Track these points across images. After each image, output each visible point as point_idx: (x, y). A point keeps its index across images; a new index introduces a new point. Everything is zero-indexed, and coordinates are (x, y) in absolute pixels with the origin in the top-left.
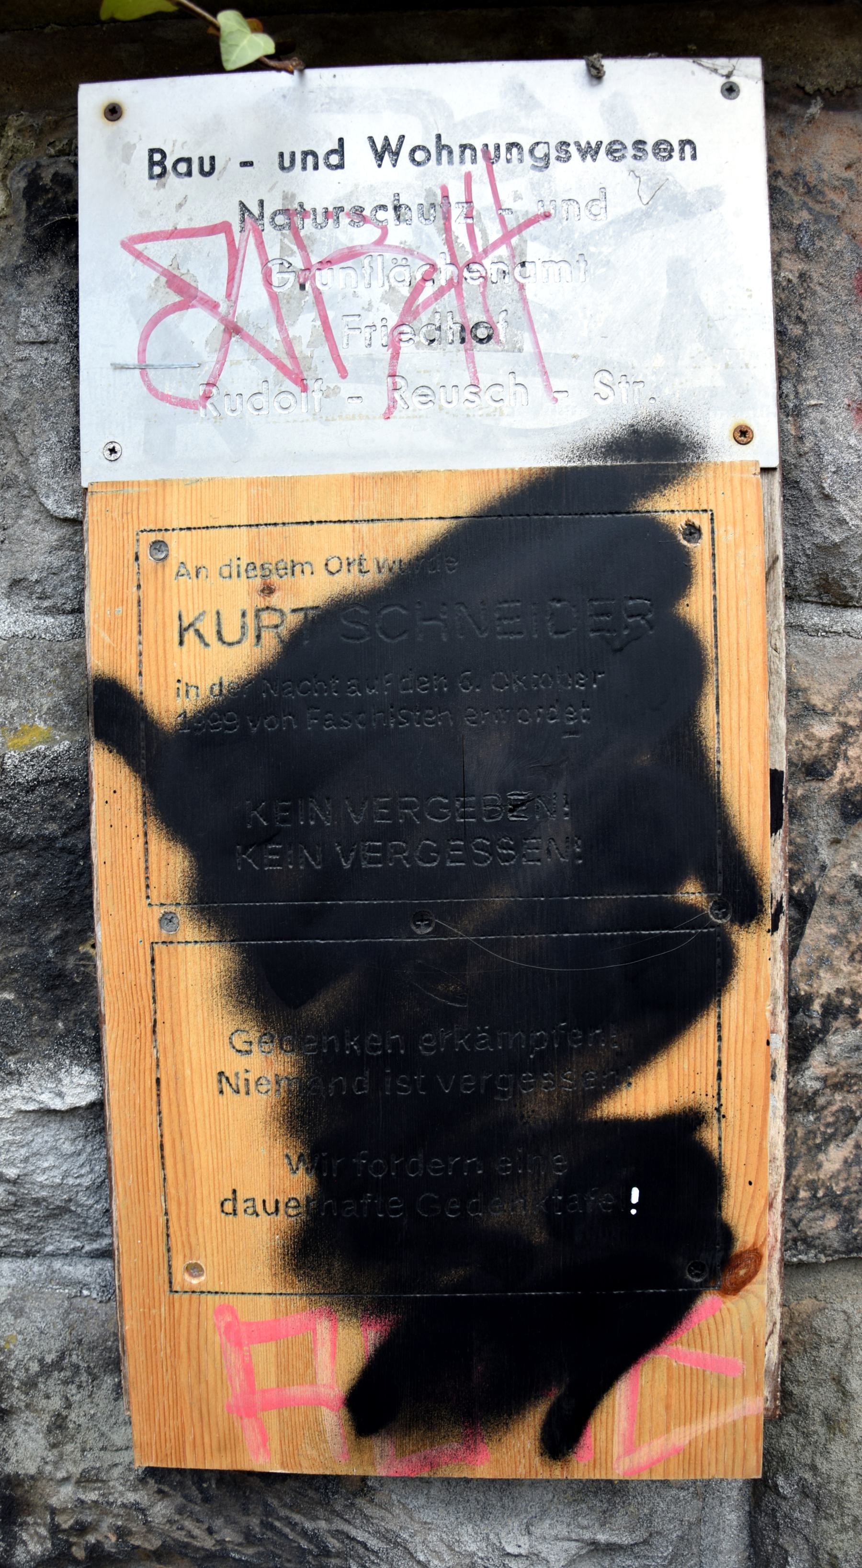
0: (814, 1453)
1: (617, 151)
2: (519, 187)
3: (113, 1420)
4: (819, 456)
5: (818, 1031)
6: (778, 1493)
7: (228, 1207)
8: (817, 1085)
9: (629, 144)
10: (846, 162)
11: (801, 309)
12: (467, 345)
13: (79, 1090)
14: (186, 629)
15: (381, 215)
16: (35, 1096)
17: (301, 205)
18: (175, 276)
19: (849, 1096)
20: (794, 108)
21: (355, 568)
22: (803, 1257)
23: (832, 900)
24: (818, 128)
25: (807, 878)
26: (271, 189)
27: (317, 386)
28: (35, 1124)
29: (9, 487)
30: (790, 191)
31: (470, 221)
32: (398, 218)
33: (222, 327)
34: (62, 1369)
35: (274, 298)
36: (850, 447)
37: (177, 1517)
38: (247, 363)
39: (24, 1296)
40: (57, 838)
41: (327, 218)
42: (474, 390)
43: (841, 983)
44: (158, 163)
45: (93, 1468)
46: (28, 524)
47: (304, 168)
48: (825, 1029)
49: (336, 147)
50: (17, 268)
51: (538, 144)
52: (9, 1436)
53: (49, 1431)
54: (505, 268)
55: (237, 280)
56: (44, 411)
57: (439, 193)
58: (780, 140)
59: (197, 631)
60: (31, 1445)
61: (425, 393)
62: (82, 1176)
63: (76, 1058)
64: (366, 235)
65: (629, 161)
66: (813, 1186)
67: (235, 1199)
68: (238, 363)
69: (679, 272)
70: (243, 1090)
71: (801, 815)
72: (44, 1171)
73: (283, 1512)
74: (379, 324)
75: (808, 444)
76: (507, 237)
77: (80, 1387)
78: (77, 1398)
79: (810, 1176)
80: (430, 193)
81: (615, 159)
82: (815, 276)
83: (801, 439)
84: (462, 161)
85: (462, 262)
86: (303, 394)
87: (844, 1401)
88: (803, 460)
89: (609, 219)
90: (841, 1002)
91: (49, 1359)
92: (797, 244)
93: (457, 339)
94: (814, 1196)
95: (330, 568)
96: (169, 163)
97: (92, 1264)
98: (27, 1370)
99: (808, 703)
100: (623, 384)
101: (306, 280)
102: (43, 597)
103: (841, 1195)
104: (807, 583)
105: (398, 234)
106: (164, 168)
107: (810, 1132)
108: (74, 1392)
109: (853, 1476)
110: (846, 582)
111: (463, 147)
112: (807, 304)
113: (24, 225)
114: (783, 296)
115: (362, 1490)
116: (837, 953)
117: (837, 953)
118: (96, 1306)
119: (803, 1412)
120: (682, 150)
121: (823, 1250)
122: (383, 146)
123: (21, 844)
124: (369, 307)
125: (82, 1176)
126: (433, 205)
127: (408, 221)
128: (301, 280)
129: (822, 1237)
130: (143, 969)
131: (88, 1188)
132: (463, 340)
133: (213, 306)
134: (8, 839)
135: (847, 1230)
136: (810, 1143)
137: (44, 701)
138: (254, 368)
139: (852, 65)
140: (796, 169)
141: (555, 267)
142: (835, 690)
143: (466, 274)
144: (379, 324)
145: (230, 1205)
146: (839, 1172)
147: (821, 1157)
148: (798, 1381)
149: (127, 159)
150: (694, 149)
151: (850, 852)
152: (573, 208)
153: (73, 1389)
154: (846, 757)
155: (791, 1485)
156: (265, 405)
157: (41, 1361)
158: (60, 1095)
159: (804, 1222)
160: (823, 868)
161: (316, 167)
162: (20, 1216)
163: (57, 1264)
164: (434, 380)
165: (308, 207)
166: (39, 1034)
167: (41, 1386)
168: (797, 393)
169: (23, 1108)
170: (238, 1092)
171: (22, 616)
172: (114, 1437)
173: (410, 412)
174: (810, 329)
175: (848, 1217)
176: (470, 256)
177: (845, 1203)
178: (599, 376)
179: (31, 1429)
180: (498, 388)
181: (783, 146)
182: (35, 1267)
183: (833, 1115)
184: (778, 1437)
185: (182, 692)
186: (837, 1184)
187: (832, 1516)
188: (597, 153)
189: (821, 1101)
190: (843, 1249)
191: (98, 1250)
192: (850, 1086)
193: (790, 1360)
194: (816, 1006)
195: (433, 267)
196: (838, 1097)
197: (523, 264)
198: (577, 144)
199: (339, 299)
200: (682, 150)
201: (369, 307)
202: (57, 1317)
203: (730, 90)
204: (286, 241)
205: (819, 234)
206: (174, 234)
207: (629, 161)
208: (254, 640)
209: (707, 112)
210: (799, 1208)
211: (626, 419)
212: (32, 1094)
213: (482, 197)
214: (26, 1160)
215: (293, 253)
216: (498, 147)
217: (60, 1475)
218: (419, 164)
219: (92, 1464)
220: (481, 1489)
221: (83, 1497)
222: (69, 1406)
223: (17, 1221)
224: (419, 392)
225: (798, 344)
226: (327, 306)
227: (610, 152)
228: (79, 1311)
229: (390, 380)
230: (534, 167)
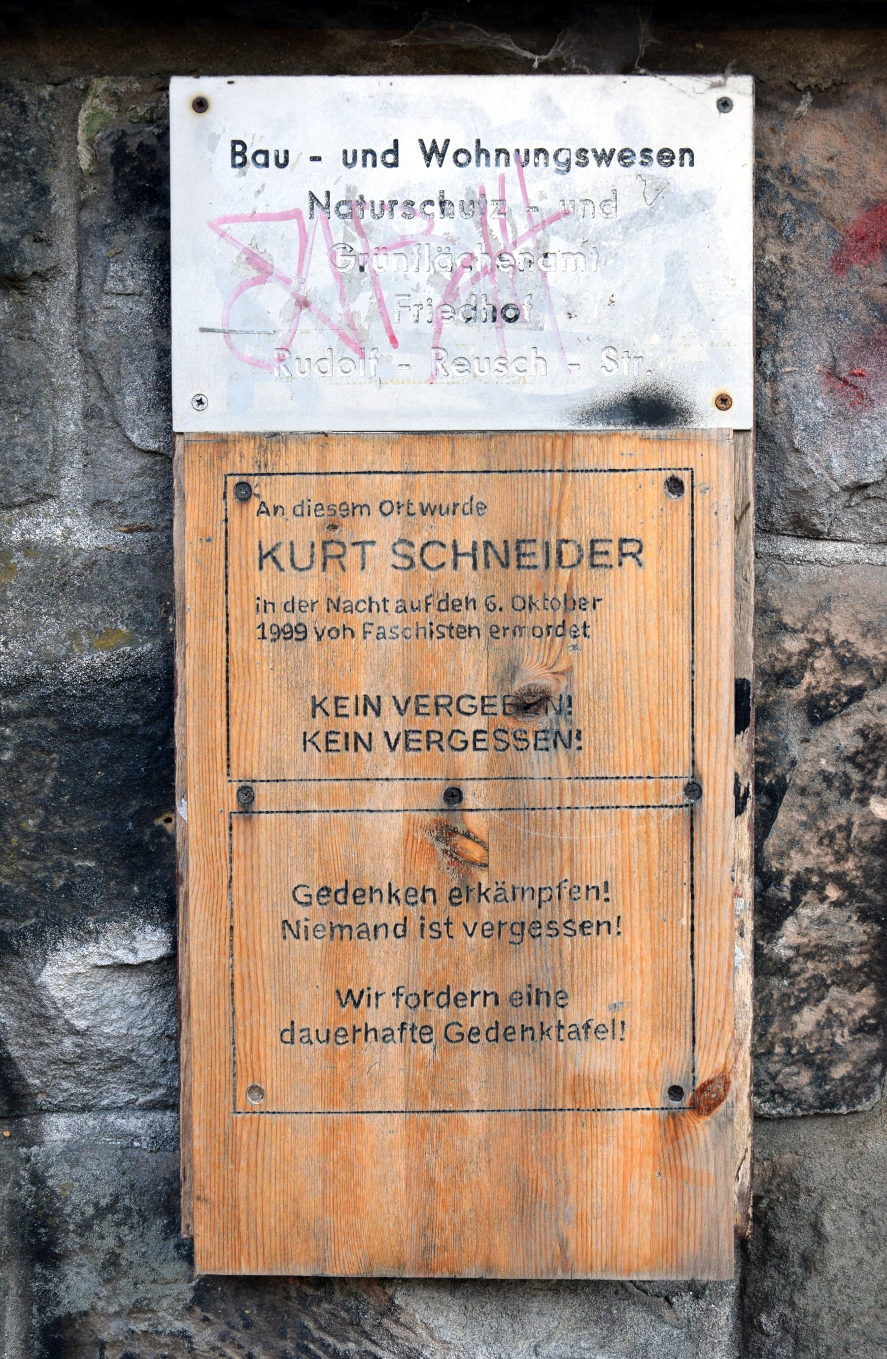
0: (793, 1291)
1: (627, 157)
2: (544, 185)
3: (162, 1257)
4: (791, 416)
5: (789, 904)
6: (762, 1332)
7: (287, 1036)
8: (790, 953)
9: (638, 152)
10: (828, 155)
11: (782, 288)
12: (497, 324)
13: (150, 946)
14: (265, 557)
15: (428, 209)
16: (110, 952)
17: (362, 197)
18: (254, 254)
19: (821, 965)
20: (786, 105)
21: (403, 510)
22: (781, 1110)
23: (803, 792)
24: (805, 124)
25: (779, 771)
26: (336, 182)
27: (372, 354)
28: (106, 979)
29: (93, 417)
30: (777, 183)
31: (502, 216)
32: (443, 212)
33: (294, 301)
34: (116, 1212)
35: (339, 277)
36: (817, 408)
37: (219, 1344)
38: (315, 333)
39: (79, 1147)
40: (139, 726)
41: (383, 210)
42: (503, 361)
43: (810, 863)
44: (239, 153)
45: (145, 1299)
46: (111, 452)
47: (365, 165)
48: (796, 902)
49: (392, 147)
50: (106, 226)
51: (561, 150)
52: (61, 1281)
53: (104, 1267)
54: (530, 258)
55: (306, 260)
56: (129, 355)
57: (477, 191)
58: (771, 136)
59: (274, 559)
60: (83, 1286)
61: (462, 362)
62: (145, 1027)
63: (149, 918)
64: (414, 226)
65: (637, 167)
66: (787, 1043)
67: (293, 1030)
68: (307, 332)
69: (675, 264)
70: (302, 935)
71: (773, 717)
72: (111, 1022)
73: (317, 1334)
74: (425, 303)
75: (782, 405)
76: (533, 230)
77: (132, 1228)
78: (129, 1238)
79: (785, 1035)
80: (469, 191)
81: (625, 165)
82: (796, 258)
83: (775, 401)
84: (497, 164)
85: (495, 252)
86: (362, 361)
87: (819, 1244)
88: (778, 418)
89: (619, 217)
90: (809, 879)
91: (103, 1203)
92: (781, 232)
93: (490, 318)
94: (789, 1052)
95: (384, 509)
96: (249, 154)
97: (144, 1116)
98: (83, 1214)
99: (780, 622)
100: (625, 360)
101: (365, 263)
102: (124, 515)
103: (814, 1054)
104: (783, 520)
105: (443, 226)
106: (245, 158)
107: (784, 995)
108: (126, 1232)
109: (827, 1310)
110: (816, 520)
111: (499, 151)
112: (788, 282)
113: (112, 188)
114: (766, 277)
115: (390, 1309)
116: (807, 837)
117: (807, 837)
118: (146, 1155)
119: (783, 1255)
120: (682, 158)
121: (799, 1104)
122: (431, 149)
123: (107, 732)
124: (417, 289)
125: (145, 1027)
126: (472, 202)
127: (452, 216)
128: (361, 263)
129: (798, 1092)
130: (222, 835)
131: (149, 1039)
132: (494, 319)
133: (287, 281)
134: (94, 727)
135: (820, 1086)
136: (785, 1004)
137: (125, 607)
138: (320, 337)
139: (838, 67)
140: (783, 164)
141: (572, 259)
142: (805, 612)
143: (498, 262)
144: (425, 303)
145: (290, 1034)
146: (812, 1033)
147: (796, 1018)
148: (780, 1227)
149: (212, 148)
150: (692, 156)
151: (819, 750)
152: (589, 207)
153: (125, 1229)
154: (813, 669)
155: (773, 1322)
156: (329, 368)
157: (96, 1205)
158: (134, 951)
159: (781, 1076)
160: (793, 763)
161: (374, 165)
162: (84, 1068)
163: (111, 1118)
164: (470, 353)
165: (367, 199)
166: (117, 897)
167: (96, 1228)
168: (774, 361)
169: (99, 963)
170: (298, 937)
171: (103, 532)
172: (164, 1272)
173: (449, 379)
174: (789, 305)
175: (820, 1074)
176: (502, 247)
177: (818, 1061)
178: (606, 352)
179: (84, 1271)
180: (523, 361)
181: (774, 141)
182: (91, 1121)
183: (806, 981)
184: (763, 1280)
185: (261, 608)
186: (810, 1044)
187: (808, 1347)
188: (610, 159)
189: (795, 968)
190: (817, 1104)
191: (151, 1101)
192: (822, 956)
193: (773, 1209)
194: (787, 881)
195: (472, 256)
196: (810, 965)
197: (546, 255)
198: (594, 151)
199: (392, 281)
200: (682, 158)
201: (417, 289)
202: (111, 1165)
203: (725, 105)
204: (349, 228)
205: (799, 222)
206: (253, 217)
207: (637, 167)
208: (321, 568)
209: (704, 122)
210: (776, 1062)
211: (627, 388)
212: (107, 950)
213: (514, 197)
214: (95, 1013)
215: (354, 240)
216: (527, 152)
217: (111, 1310)
218: (461, 165)
219: (144, 1295)
220: (495, 1315)
221: (133, 1328)
222: (121, 1244)
223: (78, 1074)
224: (458, 362)
225: (778, 319)
226: (382, 286)
227: (621, 158)
228: (131, 1159)
229: (433, 352)
230: (558, 171)
